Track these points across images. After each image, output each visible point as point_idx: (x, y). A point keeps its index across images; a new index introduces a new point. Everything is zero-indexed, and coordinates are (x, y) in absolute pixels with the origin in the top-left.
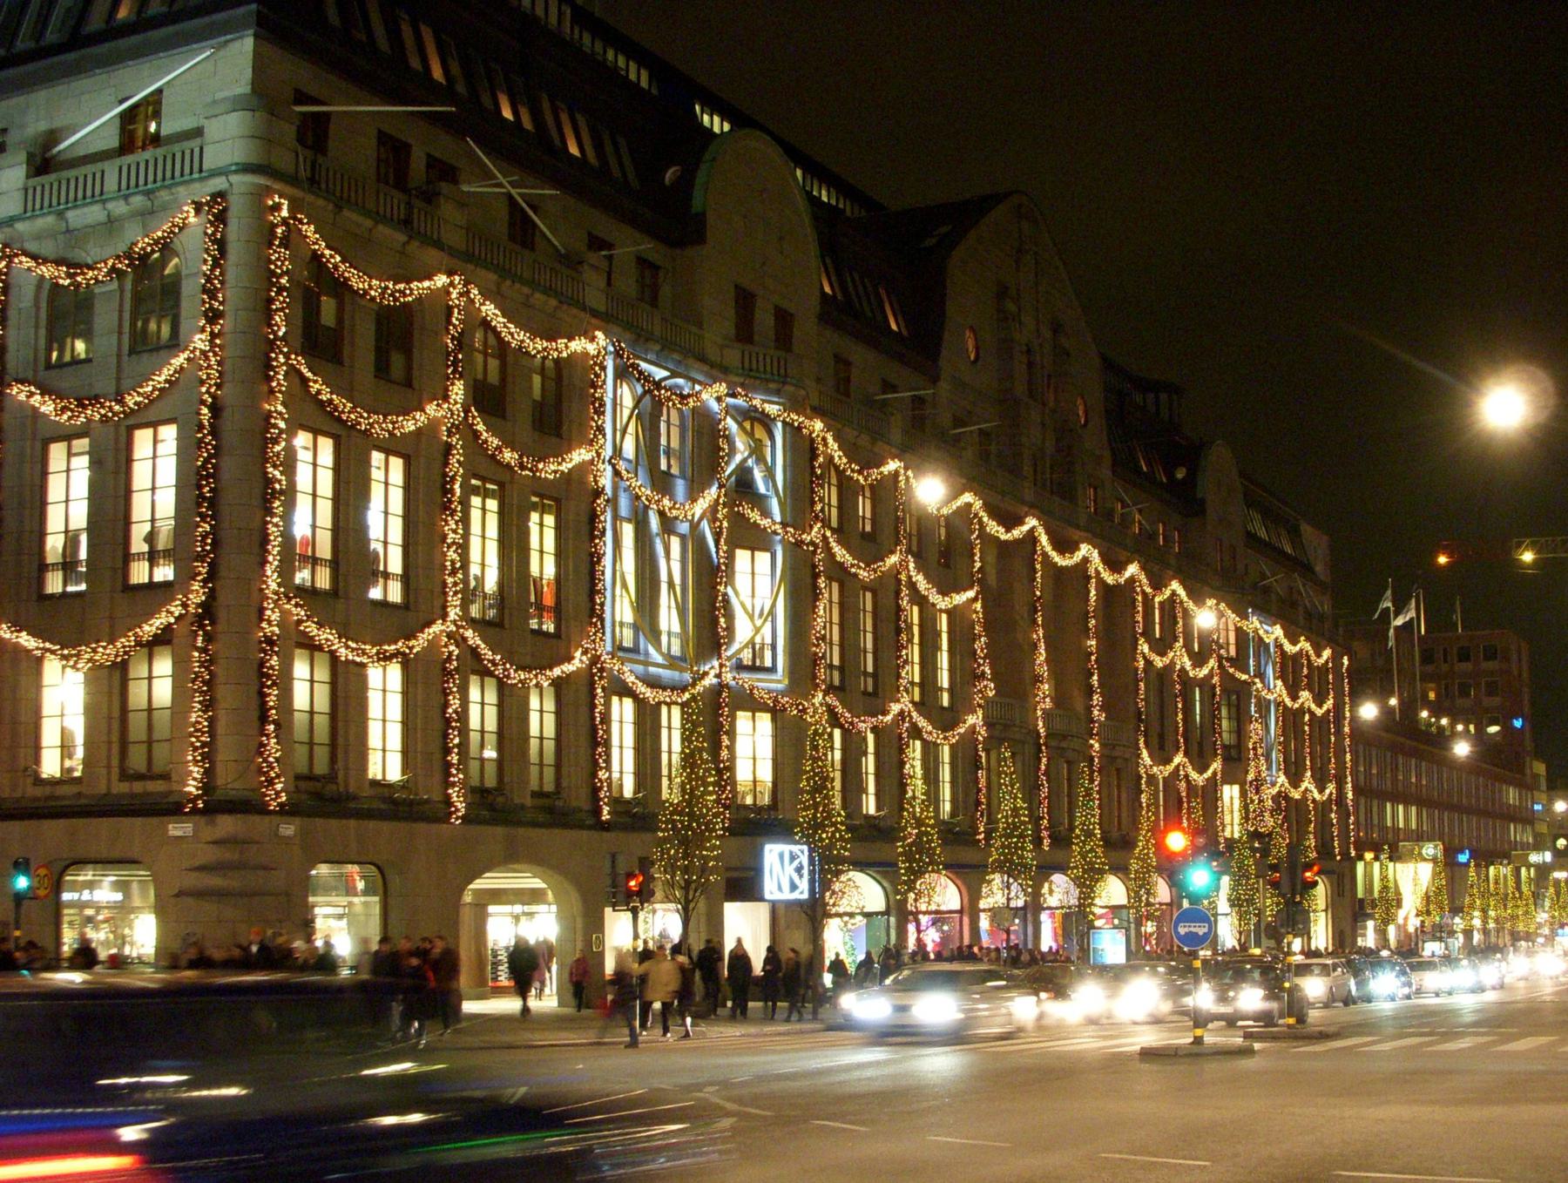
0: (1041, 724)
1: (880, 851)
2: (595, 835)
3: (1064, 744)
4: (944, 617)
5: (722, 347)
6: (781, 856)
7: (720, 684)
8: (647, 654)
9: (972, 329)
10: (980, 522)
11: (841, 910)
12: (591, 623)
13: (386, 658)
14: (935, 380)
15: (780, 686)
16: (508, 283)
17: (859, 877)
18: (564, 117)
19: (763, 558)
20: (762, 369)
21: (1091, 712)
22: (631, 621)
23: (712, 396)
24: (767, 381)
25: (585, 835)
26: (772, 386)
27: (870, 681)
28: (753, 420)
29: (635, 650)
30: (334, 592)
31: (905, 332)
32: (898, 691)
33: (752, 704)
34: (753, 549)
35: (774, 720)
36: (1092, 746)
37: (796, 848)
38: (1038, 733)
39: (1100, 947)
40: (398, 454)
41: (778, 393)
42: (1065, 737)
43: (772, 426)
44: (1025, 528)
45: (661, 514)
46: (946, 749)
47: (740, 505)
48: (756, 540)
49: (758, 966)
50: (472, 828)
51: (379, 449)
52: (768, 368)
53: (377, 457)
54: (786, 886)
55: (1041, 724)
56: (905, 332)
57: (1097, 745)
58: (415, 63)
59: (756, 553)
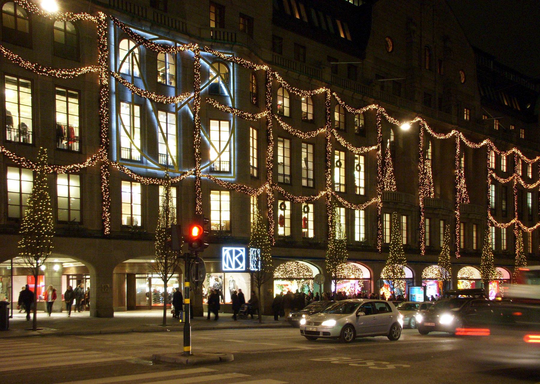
0: (421, 203)
1: (317, 253)
2: (104, 241)
3: (436, 212)
4: (530, 195)
5: (200, 29)
6: (231, 252)
7: (196, 178)
8: (147, 163)
9: (389, 37)
10: (384, 118)
11: (428, 277)
12: (100, 147)
13: (308, 202)
14: (362, 57)
15: (233, 179)
16: (365, 97)
17: (499, 269)
18: (503, 96)
19: (225, 125)
20: (222, 38)
21: (456, 200)
22: (344, 183)
23: (190, 50)
24: (224, 44)
25: (97, 241)
26: (227, 46)
27: (255, 171)
28: (219, 62)
29: (141, 162)
30: (346, 192)
31: (349, 38)
32: (326, 187)
33: (219, 187)
34: (220, 120)
35: (231, 194)
36: (456, 213)
37: (239, 249)
38: (420, 208)
39: (413, 294)
40: (310, 144)
41: (231, 49)
42: (435, 209)
43: (229, 65)
44: (451, 134)
45: (151, 100)
46: (505, 229)
47: (208, 99)
48: (221, 116)
49: (247, 298)
50: (59, 238)
51: (305, 142)
52: (226, 38)
53: (304, 145)
54: (233, 265)
55: (421, 203)
56: (349, 38)
57: (458, 213)
58: (515, 107)
59: (221, 122)
